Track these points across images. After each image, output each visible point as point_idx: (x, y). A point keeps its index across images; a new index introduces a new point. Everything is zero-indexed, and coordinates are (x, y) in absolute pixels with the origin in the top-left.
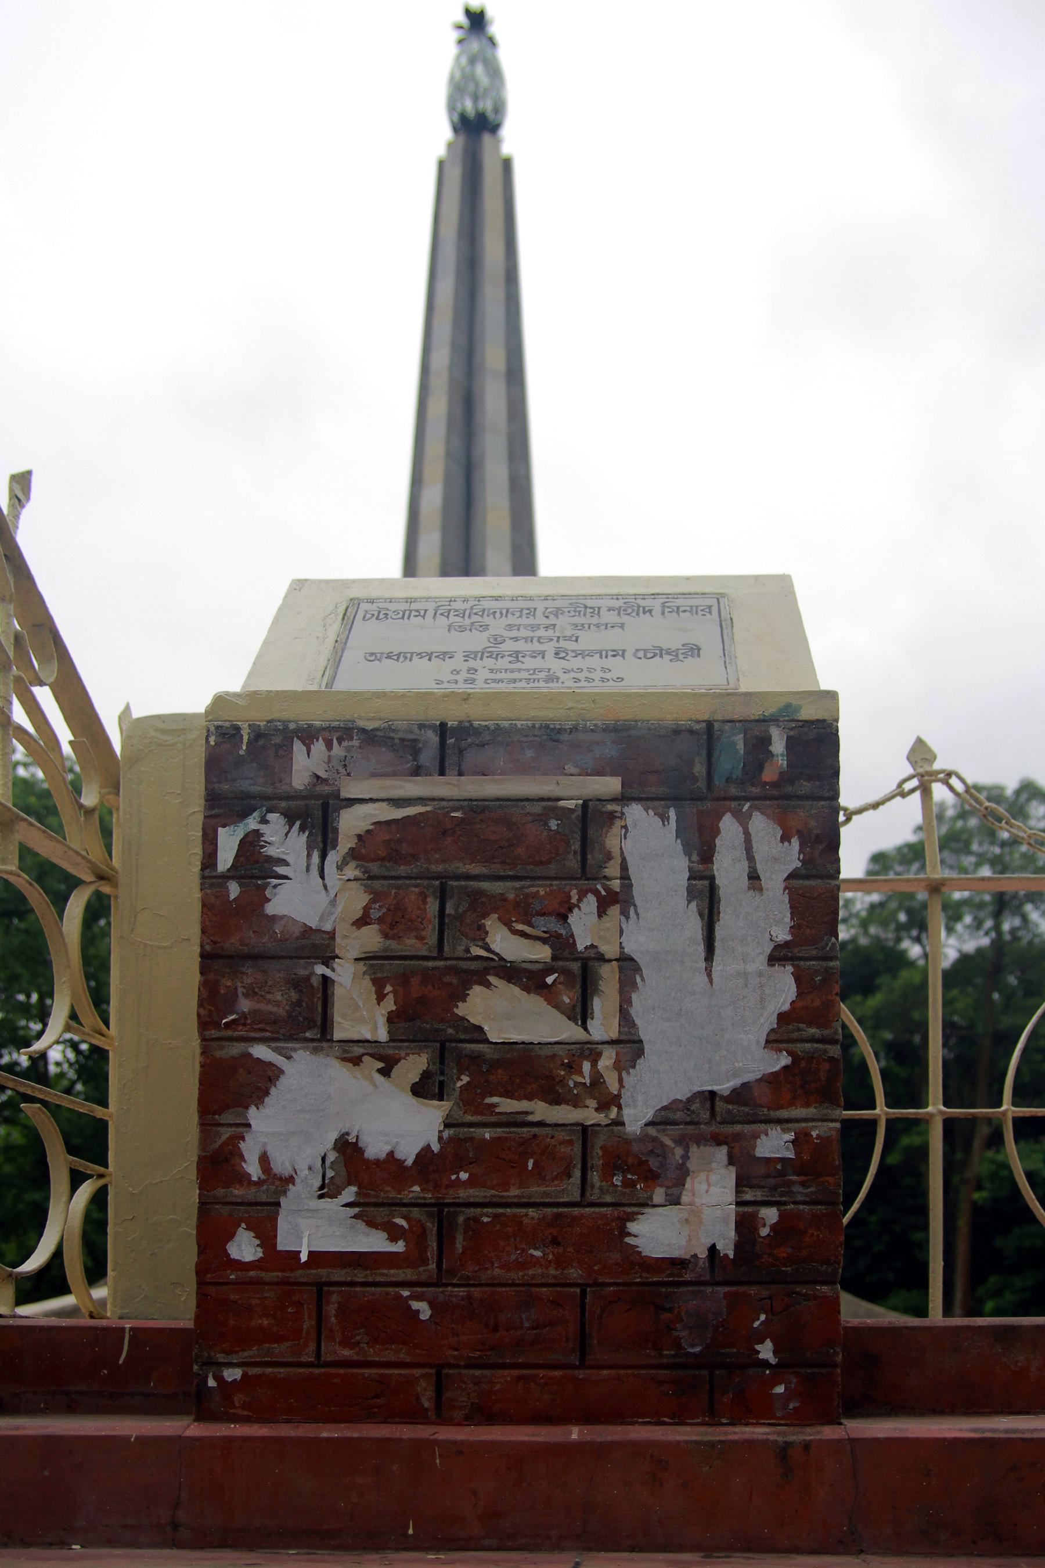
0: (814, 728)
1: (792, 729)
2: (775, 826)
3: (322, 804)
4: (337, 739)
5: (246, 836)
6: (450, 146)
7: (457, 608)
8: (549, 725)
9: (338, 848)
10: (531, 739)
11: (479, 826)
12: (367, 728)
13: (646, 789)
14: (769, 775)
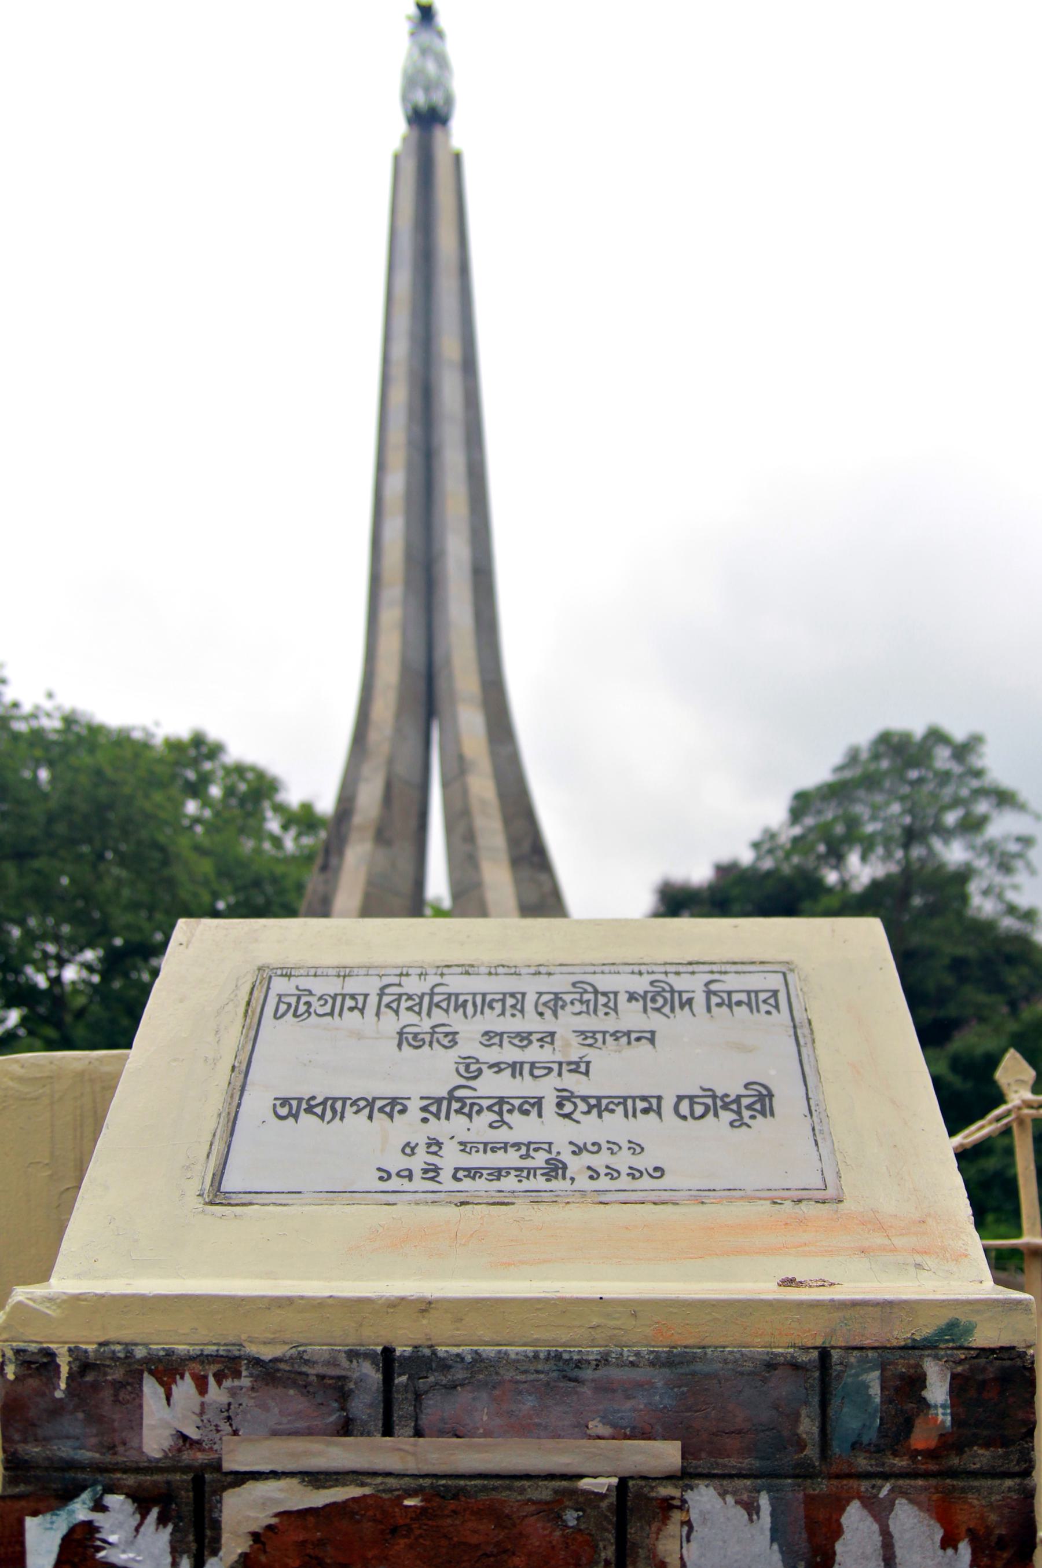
0: (996, 1359)
1: (961, 1362)
2: (932, 1522)
3: (193, 1479)
4: (215, 1375)
5: (72, 1530)
6: (405, 140)
7: (411, 992)
8: (561, 1353)
9: (221, 1554)
10: (531, 1377)
11: (449, 1521)
12: (263, 1357)
13: (720, 1461)
14: (921, 1438)
